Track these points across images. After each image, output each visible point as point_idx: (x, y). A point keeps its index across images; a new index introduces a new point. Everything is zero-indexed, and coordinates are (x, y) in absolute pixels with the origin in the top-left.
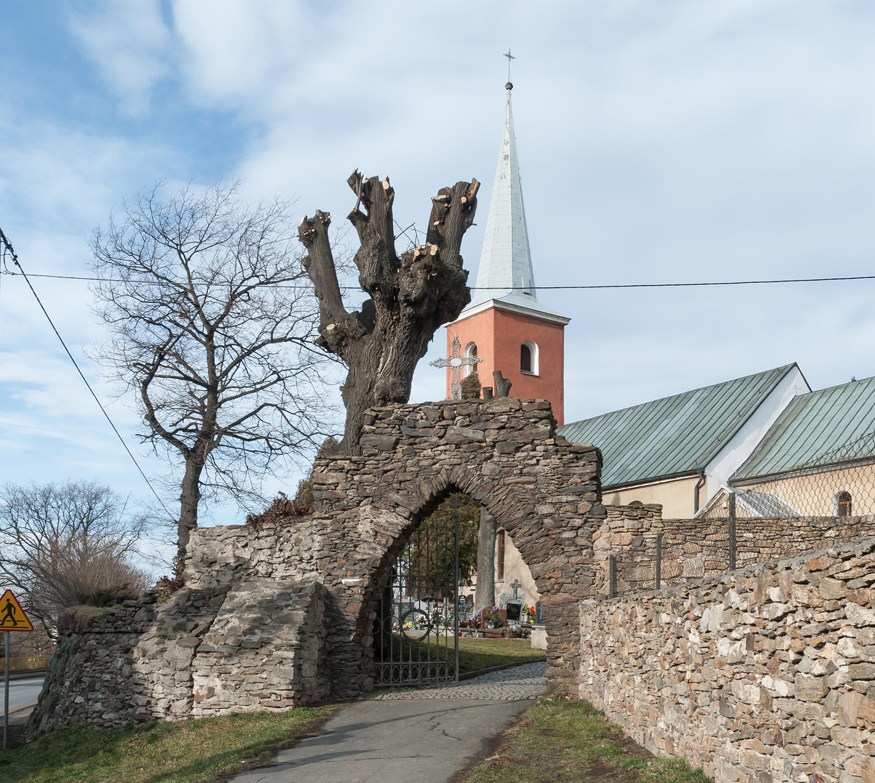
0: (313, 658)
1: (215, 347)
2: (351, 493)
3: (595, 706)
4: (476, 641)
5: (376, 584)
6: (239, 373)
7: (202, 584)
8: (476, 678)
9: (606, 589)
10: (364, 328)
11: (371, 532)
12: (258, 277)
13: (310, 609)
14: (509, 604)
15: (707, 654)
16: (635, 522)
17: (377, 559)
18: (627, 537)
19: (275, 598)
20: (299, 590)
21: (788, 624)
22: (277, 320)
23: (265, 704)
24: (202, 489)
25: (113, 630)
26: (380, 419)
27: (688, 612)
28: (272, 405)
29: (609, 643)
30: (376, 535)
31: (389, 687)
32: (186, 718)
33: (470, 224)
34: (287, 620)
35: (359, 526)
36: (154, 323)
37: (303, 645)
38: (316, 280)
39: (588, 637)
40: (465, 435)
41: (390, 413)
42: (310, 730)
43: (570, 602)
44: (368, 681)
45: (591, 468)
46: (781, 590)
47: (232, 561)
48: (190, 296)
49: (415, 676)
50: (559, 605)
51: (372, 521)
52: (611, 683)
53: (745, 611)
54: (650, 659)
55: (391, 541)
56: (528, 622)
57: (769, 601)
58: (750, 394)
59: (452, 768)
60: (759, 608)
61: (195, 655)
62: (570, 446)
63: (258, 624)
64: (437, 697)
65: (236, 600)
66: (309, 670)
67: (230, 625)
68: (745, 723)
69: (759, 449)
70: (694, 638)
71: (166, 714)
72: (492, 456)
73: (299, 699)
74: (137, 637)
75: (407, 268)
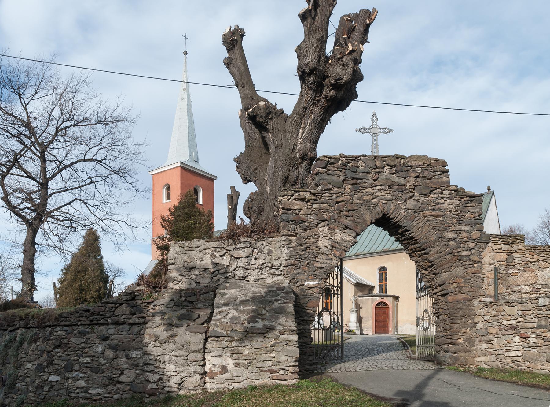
11: (329, 247)
16: (508, 246)
23: (274, 378)
25: (89, 323)
34: (281, 311)
35: (319, 242)
40: (393, 180)
61: (206, 340)
65: (227, 296)
72: (414, 196)
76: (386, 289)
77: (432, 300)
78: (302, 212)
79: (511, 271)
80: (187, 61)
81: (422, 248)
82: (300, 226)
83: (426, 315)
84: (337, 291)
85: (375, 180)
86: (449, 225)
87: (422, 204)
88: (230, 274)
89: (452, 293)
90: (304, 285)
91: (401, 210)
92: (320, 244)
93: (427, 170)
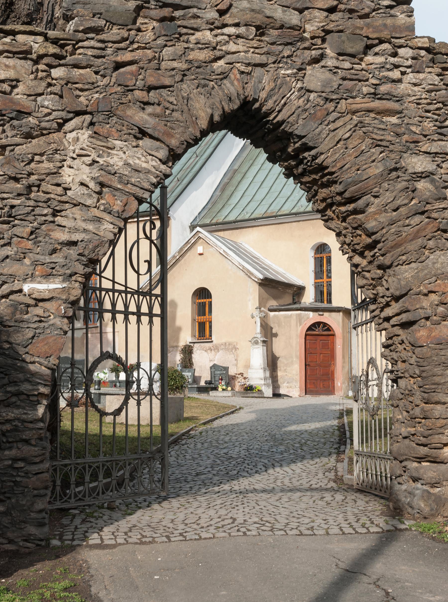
2: (48, 101)
11: (92, 185)
35: (66, 171)
40: (268, 13)
69: (218, 193)
72: (323, 56)
76: (329, 294)
77: (382, 337)
78: (21, 88)
81: (347, 195)
82: (13, 127)
83: (373, 375)
84: (151, 308)
85: (222, 13)
86: (416, 137)
87: (344, 79)
89: (427, 319)
90: (21, 291)
91: (292, 92)
92: (68, 176)
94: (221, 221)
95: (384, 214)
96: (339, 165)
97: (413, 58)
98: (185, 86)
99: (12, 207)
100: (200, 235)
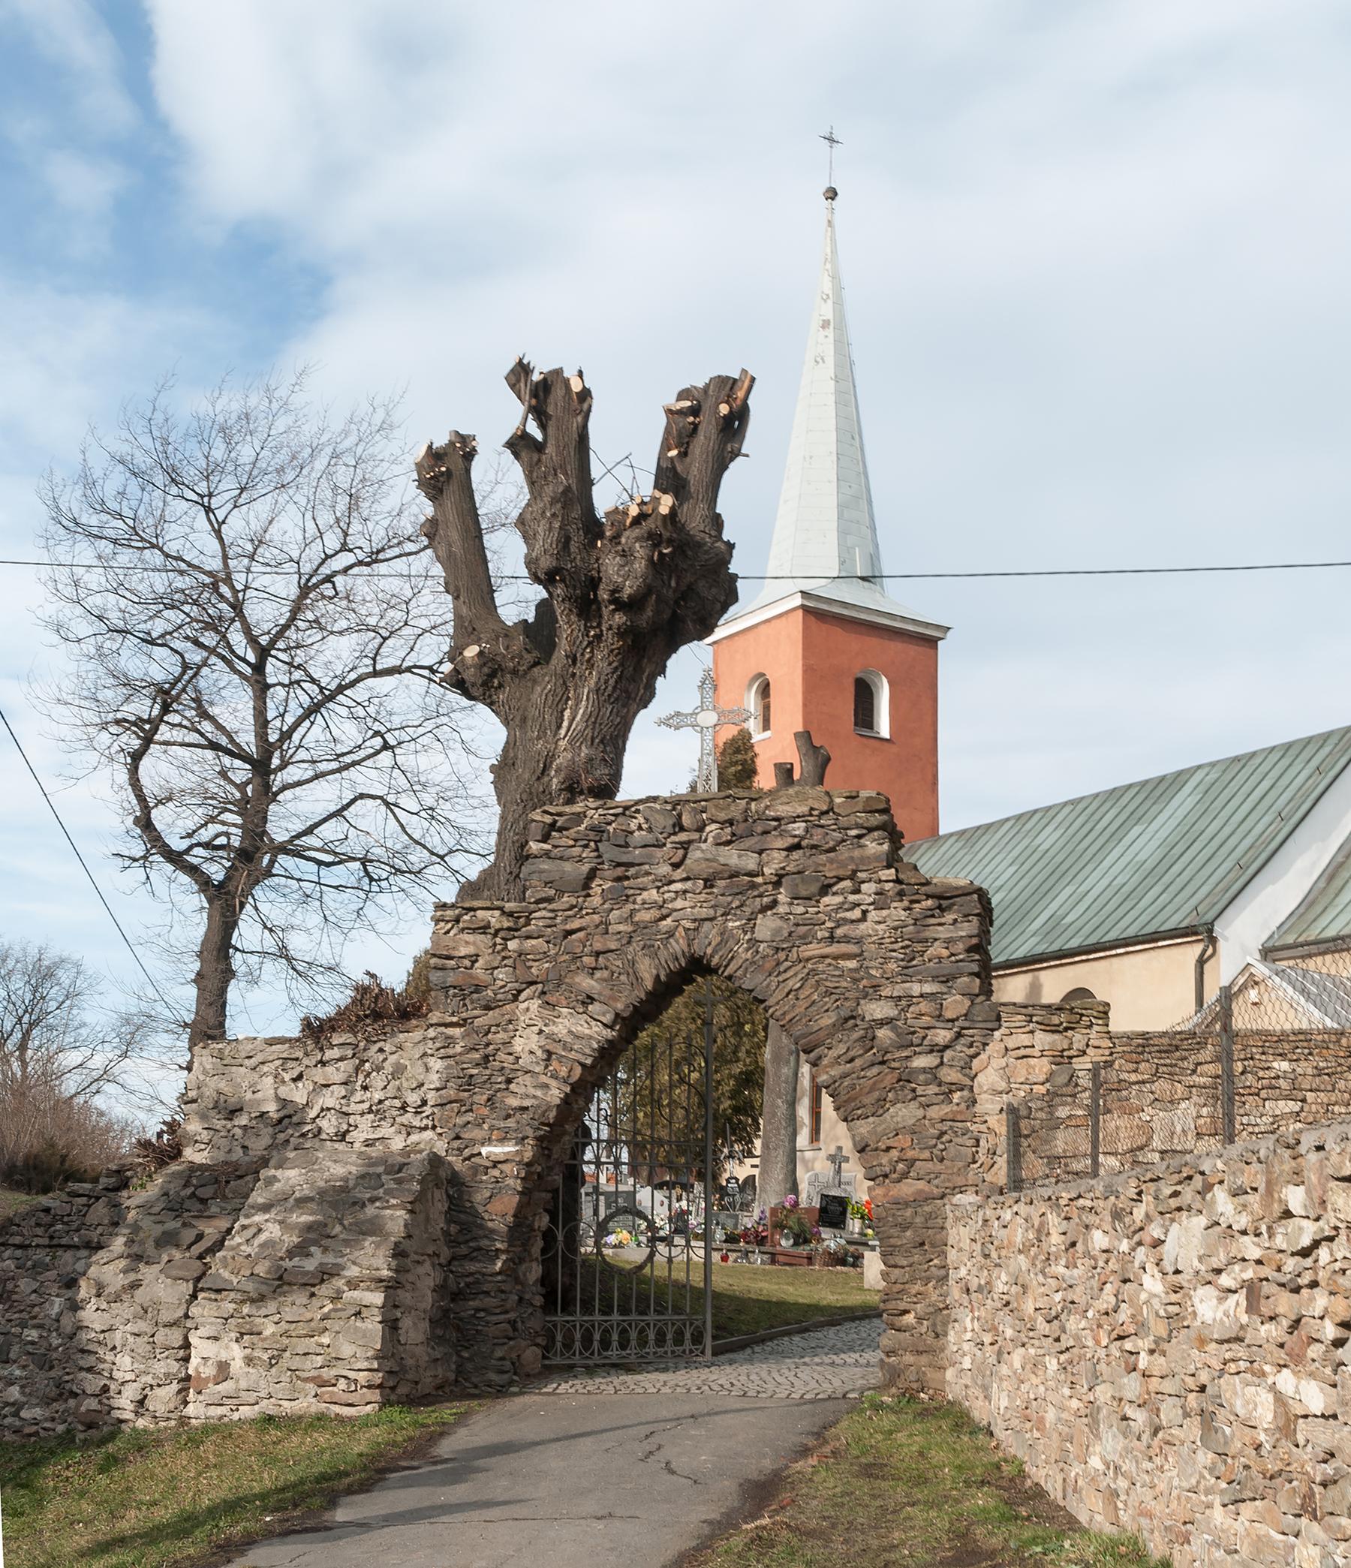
0: (422, 1306)
1: (269, 686)
2: (501, 975)
3: (976, 1414)
4: (755, 1272)
5: (549, 1156)
6: (314, 734)
7: (215, 1153)
8: (749, 1351)
9: (1000, 1174)
10: (536, 653)
11: (539, 1053)
12: (351, 550)
13: (418, 1207)
14: (824, 1197)
15: (1177, 1319)
16: (1056, 1036)
17: (549, 1108)
18: (1041, 1067)
19: (351, 1183)
20: (397, 1168)
21: (1321, 1263)
22: (385, 634)
23: (326, 1397)
24: (237, 961)
26: (560, 830)
27: (1141, 1229)
28: (374, 797)
29: (1000, 1287)
30: (548, 1059)
31: (572, 1367)
32: (173, 1423)
33: (736, 454)
34: (373, 1228)
35: (517, 1041)
36: (152, 642)
37: (402, 1278)
38: (447, 561)
39: (963, 1272)
40: (722, 860)
41: (580, 817)
42: (407, 1455)
43: (929, 1198)
44: (531, 1355)
45: (969, 929)
46: (1308, 1192)
47: (271, 1107)
48: (224, 589)
49: (623, 1345)
50: (907, 1204)
51: (541, 1032)
52: (1004, 1370)
53: (1244, 1233)
54: (1074, 1323)
55: (578, 1071)
56: (863, 1234)
57: (1287, 1214)
58: (1301, 774)
59: (675, 1543)
60: (1269, 1228)
61: (194, 1297)
62: (928, 883)
63: (315, 1236)
64: (664, 1390)
65: (277, 1186)
66: (414, 1331)
67: (263, 1237)
68: (1247, 1467)
69: (1322, 884)
70: (1153, 1284)
71: (136, 1413)
73: (393, 1388)
74: (90, 1256)
75: (616, 538)
79: (1062, 1112)
80: (837, 223)
87: (798, 925)
88: (309, 1127)
90: (480, 1154)
93: (822, 826)
94: (1312, 938)
95: (837, 1067)
96: (788, 1018)
97: (876, 894)
98: (631, 949)
99: (471, 1076)
100: (1252, 970)
